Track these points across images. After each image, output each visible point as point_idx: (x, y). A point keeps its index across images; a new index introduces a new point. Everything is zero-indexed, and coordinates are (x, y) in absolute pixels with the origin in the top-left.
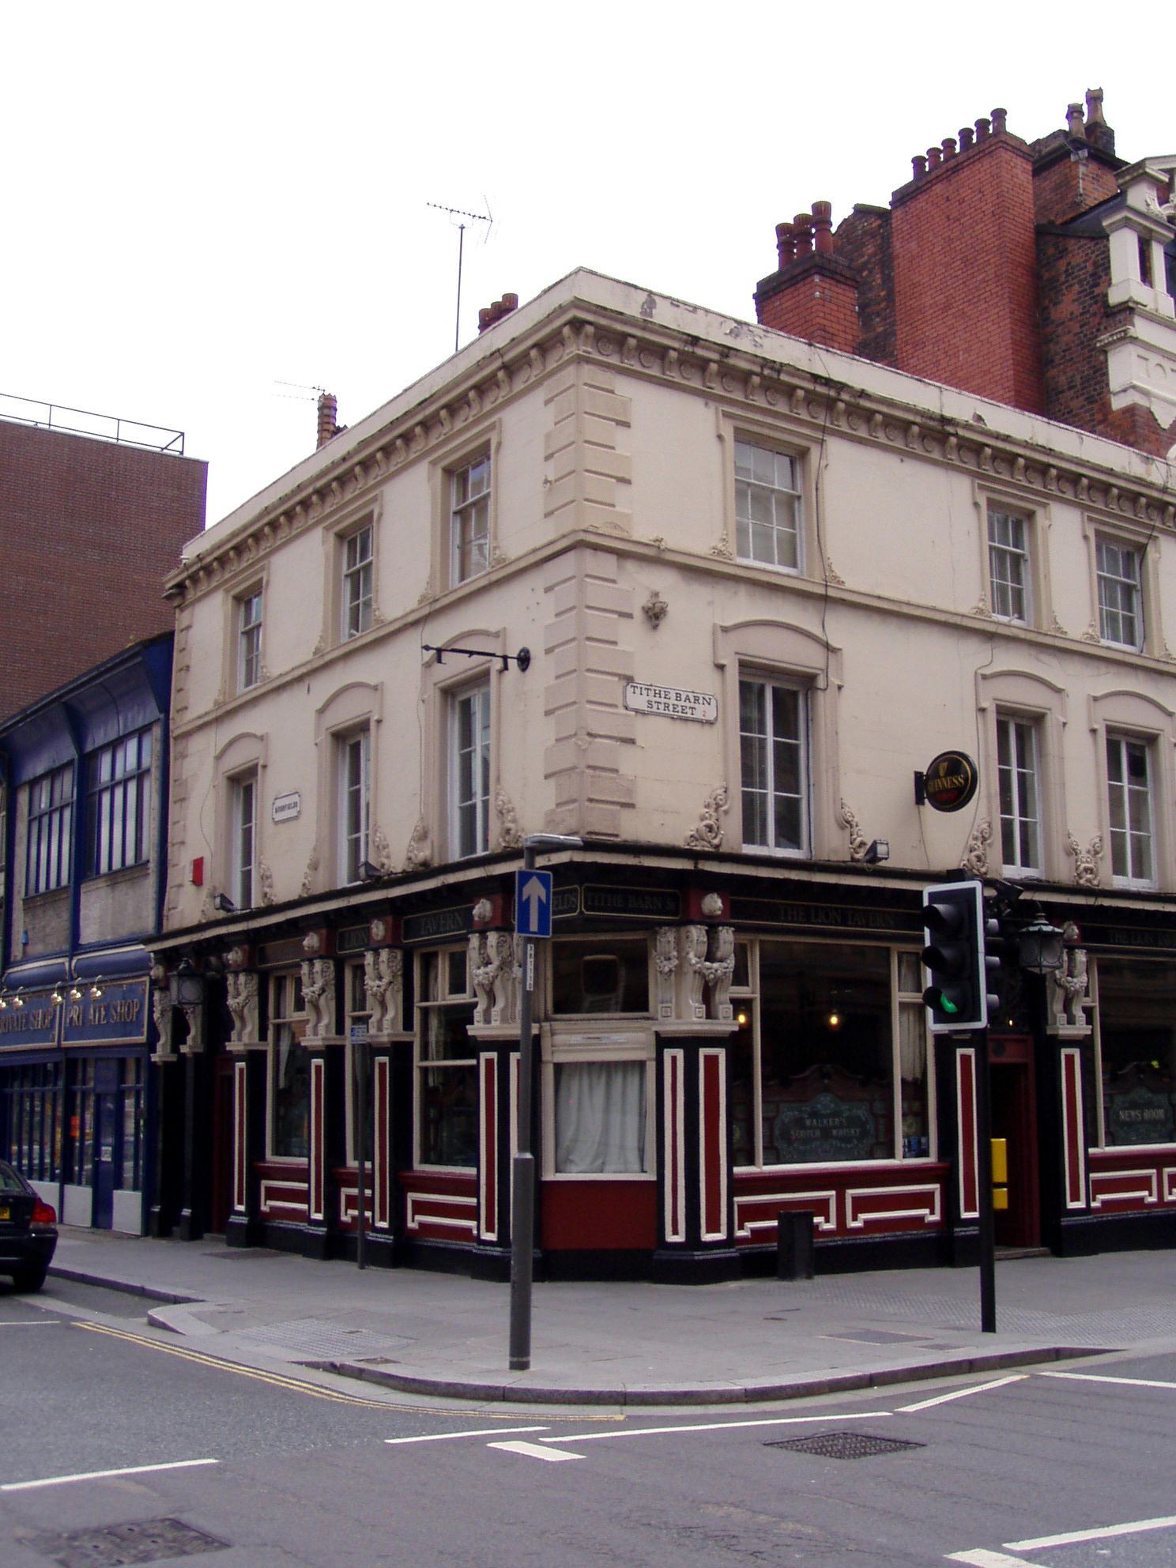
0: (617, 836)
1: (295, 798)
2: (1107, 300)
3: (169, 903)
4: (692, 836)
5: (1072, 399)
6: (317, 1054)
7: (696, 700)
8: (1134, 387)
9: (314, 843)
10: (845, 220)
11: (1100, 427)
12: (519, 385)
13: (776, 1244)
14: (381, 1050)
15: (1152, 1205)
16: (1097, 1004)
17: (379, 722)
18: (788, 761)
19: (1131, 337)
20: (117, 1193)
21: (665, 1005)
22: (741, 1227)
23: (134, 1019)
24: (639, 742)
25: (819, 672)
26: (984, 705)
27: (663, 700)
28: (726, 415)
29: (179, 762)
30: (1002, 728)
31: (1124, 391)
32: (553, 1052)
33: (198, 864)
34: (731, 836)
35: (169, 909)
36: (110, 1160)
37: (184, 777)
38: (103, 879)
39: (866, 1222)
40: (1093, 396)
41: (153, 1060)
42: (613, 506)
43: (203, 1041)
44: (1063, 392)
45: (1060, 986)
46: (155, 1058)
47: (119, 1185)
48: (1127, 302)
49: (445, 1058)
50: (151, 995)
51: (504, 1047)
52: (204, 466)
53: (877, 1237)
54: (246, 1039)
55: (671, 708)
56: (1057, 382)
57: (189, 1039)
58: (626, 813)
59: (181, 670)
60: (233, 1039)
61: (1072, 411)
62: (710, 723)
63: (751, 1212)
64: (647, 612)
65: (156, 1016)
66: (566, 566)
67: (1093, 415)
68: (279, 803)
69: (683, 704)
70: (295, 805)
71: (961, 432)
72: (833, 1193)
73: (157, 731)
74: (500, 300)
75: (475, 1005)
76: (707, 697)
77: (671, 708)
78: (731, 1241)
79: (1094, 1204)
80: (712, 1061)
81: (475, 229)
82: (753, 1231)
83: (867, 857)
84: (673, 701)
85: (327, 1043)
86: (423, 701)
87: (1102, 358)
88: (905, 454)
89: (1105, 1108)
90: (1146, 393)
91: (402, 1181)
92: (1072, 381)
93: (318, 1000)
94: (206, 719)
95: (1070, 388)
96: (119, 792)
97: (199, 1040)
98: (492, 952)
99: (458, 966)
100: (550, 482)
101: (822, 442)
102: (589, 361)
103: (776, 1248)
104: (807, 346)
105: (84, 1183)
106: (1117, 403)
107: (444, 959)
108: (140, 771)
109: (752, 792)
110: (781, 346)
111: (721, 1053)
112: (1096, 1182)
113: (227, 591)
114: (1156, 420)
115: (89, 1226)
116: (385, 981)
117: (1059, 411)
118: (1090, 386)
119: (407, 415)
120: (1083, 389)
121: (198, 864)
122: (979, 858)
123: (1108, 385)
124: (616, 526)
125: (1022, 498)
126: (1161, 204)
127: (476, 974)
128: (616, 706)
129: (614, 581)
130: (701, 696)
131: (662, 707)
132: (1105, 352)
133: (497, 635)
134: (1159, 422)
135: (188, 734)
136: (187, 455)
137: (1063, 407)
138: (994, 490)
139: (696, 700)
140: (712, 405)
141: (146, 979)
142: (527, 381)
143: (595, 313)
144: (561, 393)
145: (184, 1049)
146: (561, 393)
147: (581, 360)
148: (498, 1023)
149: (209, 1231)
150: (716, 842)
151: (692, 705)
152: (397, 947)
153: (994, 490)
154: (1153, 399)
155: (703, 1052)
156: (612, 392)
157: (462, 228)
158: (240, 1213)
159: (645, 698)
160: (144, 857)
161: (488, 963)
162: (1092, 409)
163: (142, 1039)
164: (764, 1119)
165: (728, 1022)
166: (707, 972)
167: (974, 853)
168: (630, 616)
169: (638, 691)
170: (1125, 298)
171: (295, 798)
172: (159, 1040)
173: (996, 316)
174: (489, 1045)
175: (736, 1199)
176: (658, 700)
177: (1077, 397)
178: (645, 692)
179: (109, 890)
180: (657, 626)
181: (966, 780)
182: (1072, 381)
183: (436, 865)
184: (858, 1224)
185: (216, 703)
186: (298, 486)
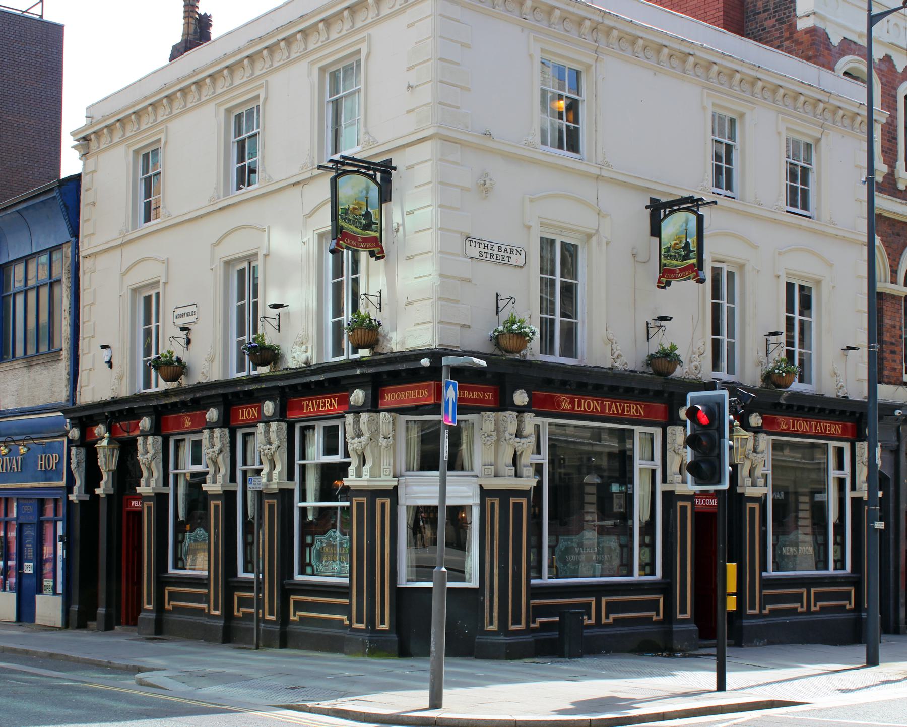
1: (193, 308)
5: (766, 19)
6: (216, 496)
7: (512, 251)
11: (786, 44)
13: (557, 633)
14: (272, 495)
15: (802, 613)
16: (771, 472)
17: (266, 255)
18: (569, 291)
20: (38, 597)
21: (487, 467)
22: (534, 622)
23: (54, 468)
27: (489, 251)
36: (31, 572)
38: (20, 361)
41: (70, 499)
43: (113, 486)
44: (759, 13)
46: (72, 497)
47: (40, 591)
50: (69, 451)
52: (58, 29)
54: (153, 484)
55: (495, 257)
56: (756, 5)
57: (102, 484)
59: (88, 204)
60: (141, 484)
61: (765, 29)
63: (538, 611)
65: (73, 467)
67: (781, 33)
68: (179, 311)
69: (503, 254)
70: (193, 313)
71: (698, 53)
72: (594, 599)
73: (68, 250)
75: (349, 464)
76: (519, 249)
77: (495, 257)
78: (529, 630)
79: (764, 612)
80: (518, 506)
82: (541, 623)
84: (496, 252)
86: (305, 243)
89: (773, 545)
90: (823, 18)
92: (767, 6)
93: (216, 458)
95: (765, 11)
96: (32, 296)
97: (110, 485)
98: (364, 427)
99: (331, 435)
100: (412, 87)
103: (557, 636)
105: (8, 590)
106: (802, 25)
108: (51, 281)
109: (572, 322)
111: (524, 501)
112: (535, 607)
114: (829, 39)
116: (274, 446)
117: (756, 28)
118: (781, 10)
119: (291, 24)
120: (775, 12)
122: (696, 368)
123: (795, 10)
130: (515, 248)
131: (489, 256)
134: (831, 41)
136: (46, 18)
137: (758, 26)
141: (65, 439)
142: (392, 7)
144: (421, 20)
145: (98, 491)
146: (421, 20)
148: (368, 477)
149: (119, 624)
151: (509, 255)
152: (282, 421)
154: (828, 23)
155: (512, 500)
158: (148, 610)
160: (57, 346)
161: (359, 435)
162: (781, 28)
163: (63, 483)
164: (549, 546)
165: (528, 482)
166: (517, 445)
169: (473, 244)
171: (193, 308)
174: (360, 492)
175: (532, 602)
176: (486, 250)
177: (770, 18)
178: (477, 245)
179: (25, 370)
182: (767, 6)
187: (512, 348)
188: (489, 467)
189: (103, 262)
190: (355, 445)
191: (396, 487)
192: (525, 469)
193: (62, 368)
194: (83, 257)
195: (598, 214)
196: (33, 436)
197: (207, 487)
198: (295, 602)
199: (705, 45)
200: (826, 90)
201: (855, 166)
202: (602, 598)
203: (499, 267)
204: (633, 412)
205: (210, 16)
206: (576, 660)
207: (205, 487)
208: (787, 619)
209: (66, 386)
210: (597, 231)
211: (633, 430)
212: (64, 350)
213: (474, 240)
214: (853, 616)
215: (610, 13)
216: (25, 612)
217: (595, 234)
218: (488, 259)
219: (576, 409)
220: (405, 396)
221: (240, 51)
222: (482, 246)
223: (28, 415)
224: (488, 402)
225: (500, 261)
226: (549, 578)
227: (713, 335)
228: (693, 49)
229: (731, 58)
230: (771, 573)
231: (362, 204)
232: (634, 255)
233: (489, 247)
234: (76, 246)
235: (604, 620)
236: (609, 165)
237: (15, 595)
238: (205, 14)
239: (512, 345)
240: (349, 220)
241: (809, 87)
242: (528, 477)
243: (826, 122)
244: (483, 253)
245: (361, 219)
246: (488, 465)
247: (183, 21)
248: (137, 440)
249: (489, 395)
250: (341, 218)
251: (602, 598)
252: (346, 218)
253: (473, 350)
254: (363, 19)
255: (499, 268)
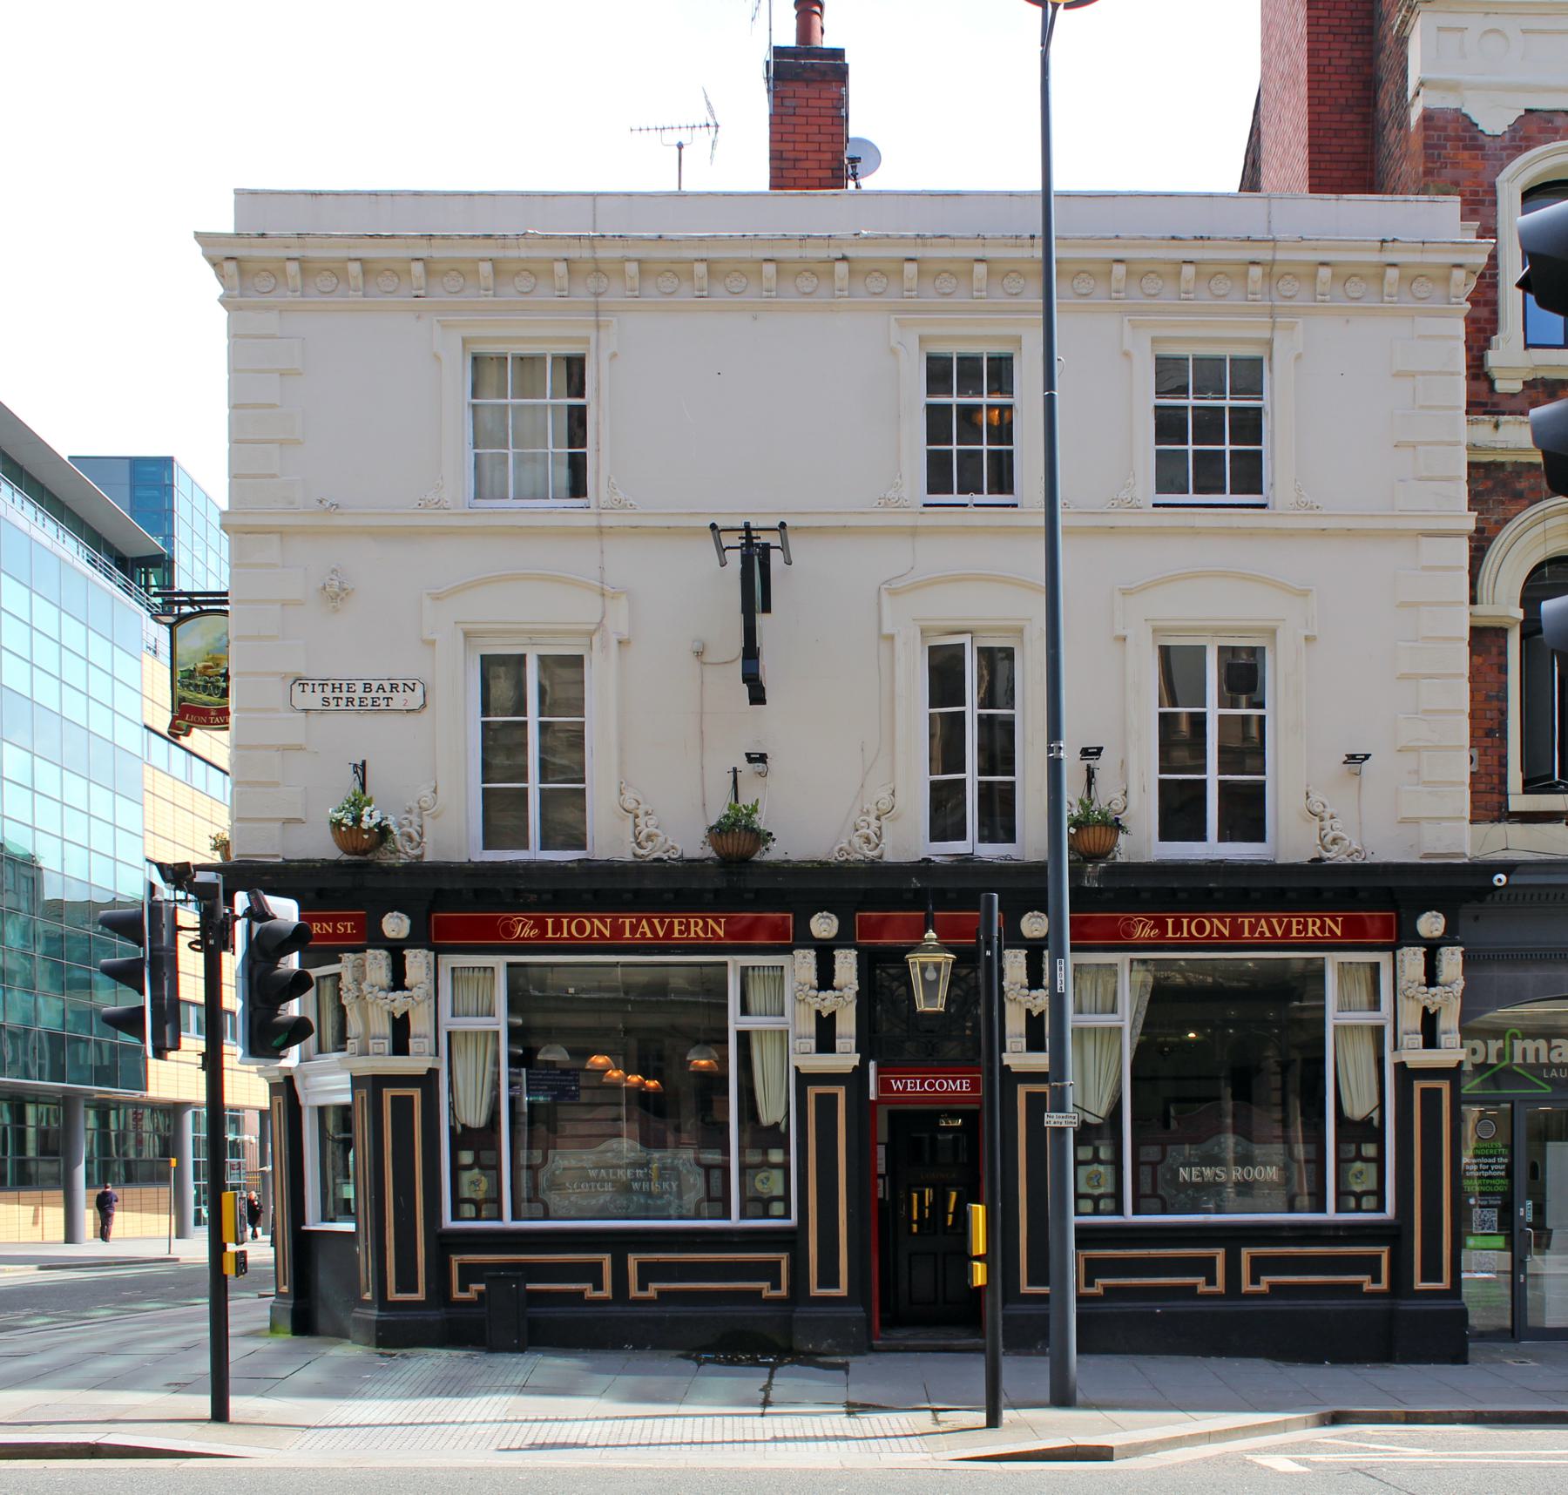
7: (394, 687)
21: (803, 1040)
39: (1272, 1286)
84: (359, 693)
94: (1401, 524)
111: (841, 1092)
114: (1477, 125)
130: (400, 683)
131: (343, 703)
139: (394, 687)
151: (388, 695)
157: (680, 146)
159: (319, 695)
173: (811, 138)
176: (337, 694)
178: (318, 689)
184: (1263, 1287)
187: (1097, 847)
188: (381, 1041)
192: (1406, 1037)
195: (603, 595)
199: (864, 232)
200: (1254, 236)
201: (1394, 375)
202: (1243, 1249)
203: (369, 718)
204: (696, 932)
206: (1494, 1344)
208: (1179, 1306)
210: (600, 624)
211: (725, 964)
213: (310, 682)
214: (798, 1309)
215: (603, 236)
217: (595, 631)
219: (1170, 934)
222: (328, 689)
224: (345, 936)
225: (369, 707)
227: (1220, 774)
228: (839, 247)
229: (947, 240)
231: (220, 659)
232: (699, 654)
233: (345, 688)
235: (1247, 1287)
236: (626, 505)
239: (1097, 841)
240: (197, 686)
241: (1200, 242)
242: (418, 1054)
243: (600, 299)
244: (331, 701)
245: (218, 681)
246: (379, 1038)
249: (346, 927)
250: (181, 685)
251: (1243, 1249)
252: (191, 684)
253: (311, 857)
255: (369, 720)
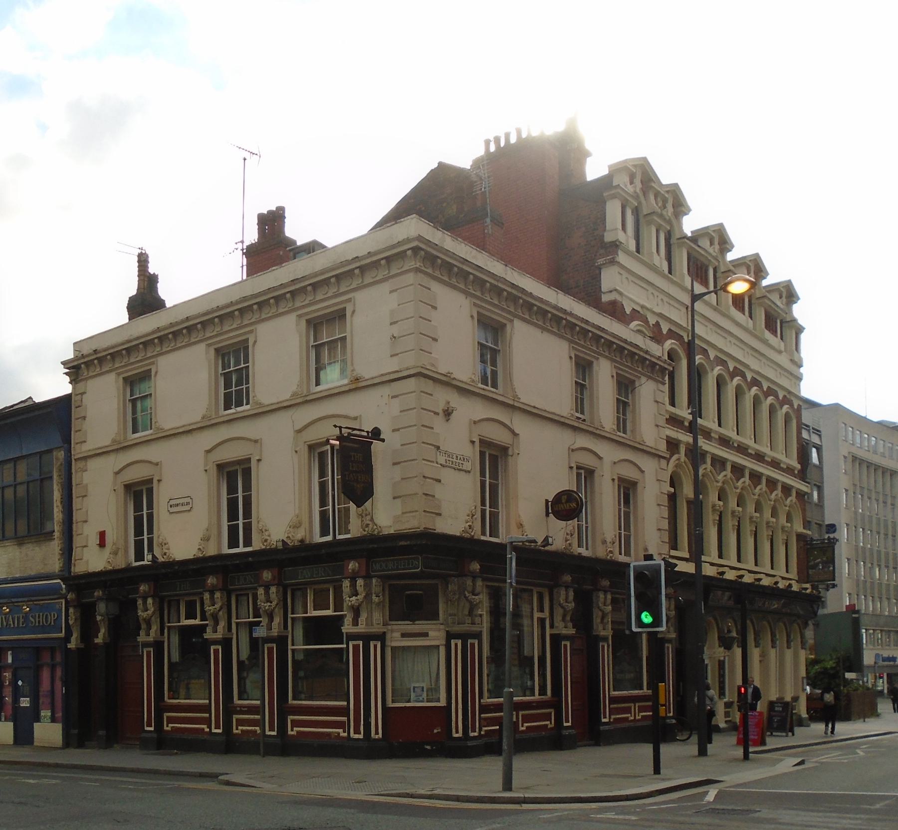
0: (435, 530)
2: (603, 239)
3: (75, 557)
4: (463, 531)
6: (215, 642)
8: (616, 290)
9: (207, 525)
10: (432, 170)
12: (368, 280)
15: (632, 721)
17: (259, 460)
19: (616, 262)
20: (36, 725)
23: (52, 623)
24: (442, 481)
25: (509, 446)
26: (572, 465)
27: (451, 459)
28: (475, 304)
29: (79, 474)
30: (579, 475)
31: (611, 292)
32: (391, 641)
33: (102, 535)
34: (477, 533)
35: (75, 560)
37: (85, 482)
39: (527, 727)
40: (590, 293)
42: (431, 353)
44: (572, 288)
45: (601, 610)
47: (38, 720)
48: (616, 241)
49: (304, 645)
51: (367, 638)
53: (532, 735)
57: (101, 635)
58: (438, 519)
62: (469, 472)
64: (444, 412)
66: (411, 383)
70: (188, 504)
71: (569, 318)
74: (275, 209)
75: (342, 618)
81: (252, 161)
83: (543, 544)
85: (280, 634)
86: (296, 452)
87: (597, 272)
88: (543, 329)
90: (621, 294)
91: (284, 711)
100: (395, 337)
101: (512, 321)
102: (421, 271)
104: (504, 266)
106: (605, 298)
107: (310, 590)
110: (494, 266)
112: (486, 719)
113: (119, 374)
115: (12, 743)
116: (274, 603)
121: (102, 535)
124: (433, 365)
125: (586, 353)
126: (631, 184)
127: (350, 601)
128: (433, 462)
129: (431, 395)
131: (451, 463)
132: (600, 269)
133: (355, 418)
135: (85, 458)
138: (579, 350)
140: (469, 298)
143: (425, 244)
147: (417, 270)
148: (363, 626)
150: (473, 534)
151: (462, 462)
153: (579, 350)
156: (430, 289)
157: (245, 159)
159: (444, 458)
163: (62, 635)
167: (568, 542)
168: (437, 414)
170: (614, 240)
172: (72, 636)
175: (482, 715)
177: (580, 293)
180: (449, 419)
181: (577, 505)
183: (308, 542)
184: (524, 728)
185: (114, 441)
186: (187, 318)
189: (92, 464)
190: (353, 602)
191: (384, 633)
193: (55, 546)
194: (75, 459)
196: (13, 600)
197: (209, 635)
198: (292, 721)
205: (157, 275)
207: (206, 636)
209: (59, 560)
212: (56, 531)
216: (23, 737)
218: (450, 465)
220: (394, 565)
221: (232, 304)
222: (447, 455)
223: (37, 581)
226: (488, 698)
230: (487, 700)
234: (69, 451)
237: (11, 724)
238: (154, 274)
247: (137, 279)
248: (137, 601)
254: (348, 285)
